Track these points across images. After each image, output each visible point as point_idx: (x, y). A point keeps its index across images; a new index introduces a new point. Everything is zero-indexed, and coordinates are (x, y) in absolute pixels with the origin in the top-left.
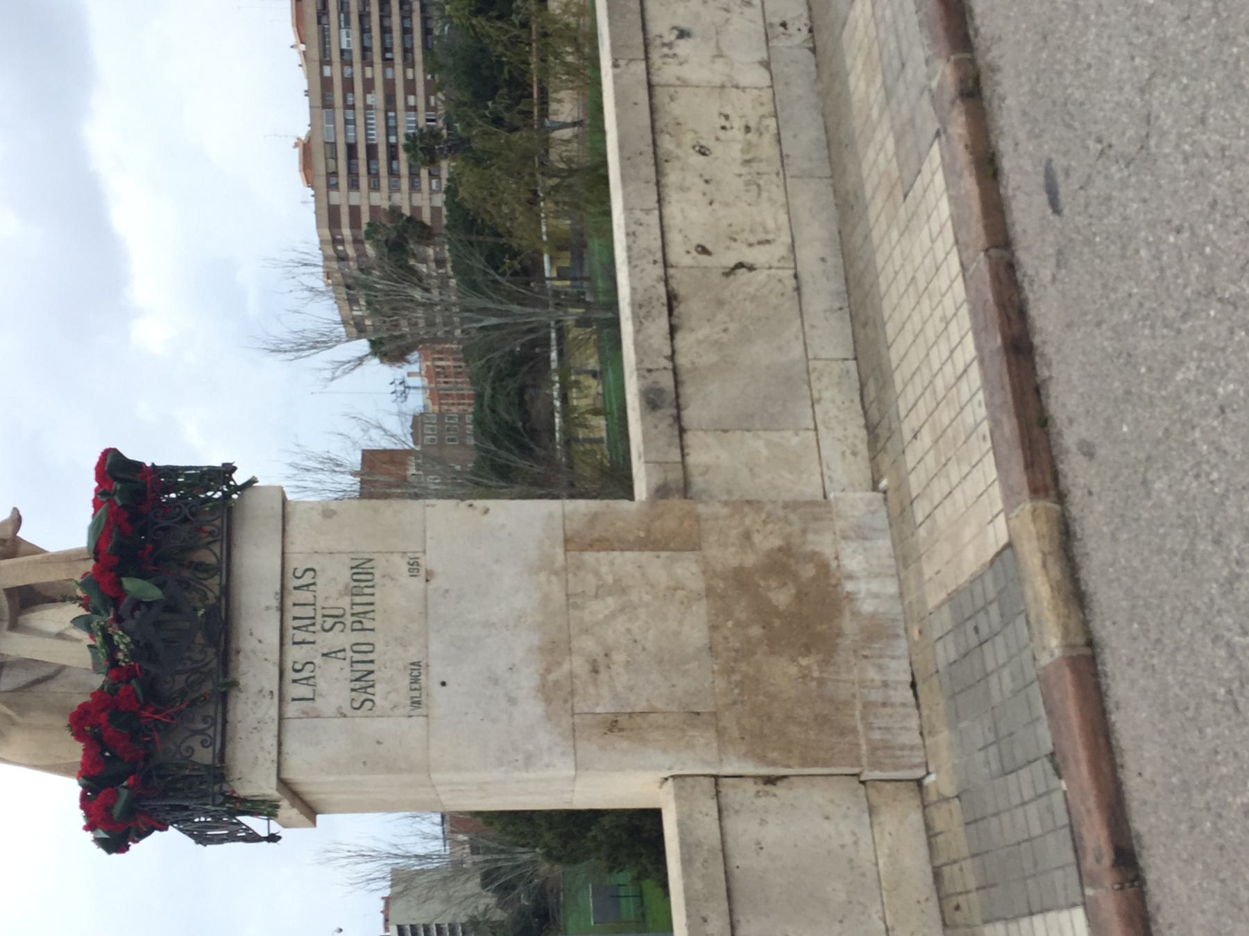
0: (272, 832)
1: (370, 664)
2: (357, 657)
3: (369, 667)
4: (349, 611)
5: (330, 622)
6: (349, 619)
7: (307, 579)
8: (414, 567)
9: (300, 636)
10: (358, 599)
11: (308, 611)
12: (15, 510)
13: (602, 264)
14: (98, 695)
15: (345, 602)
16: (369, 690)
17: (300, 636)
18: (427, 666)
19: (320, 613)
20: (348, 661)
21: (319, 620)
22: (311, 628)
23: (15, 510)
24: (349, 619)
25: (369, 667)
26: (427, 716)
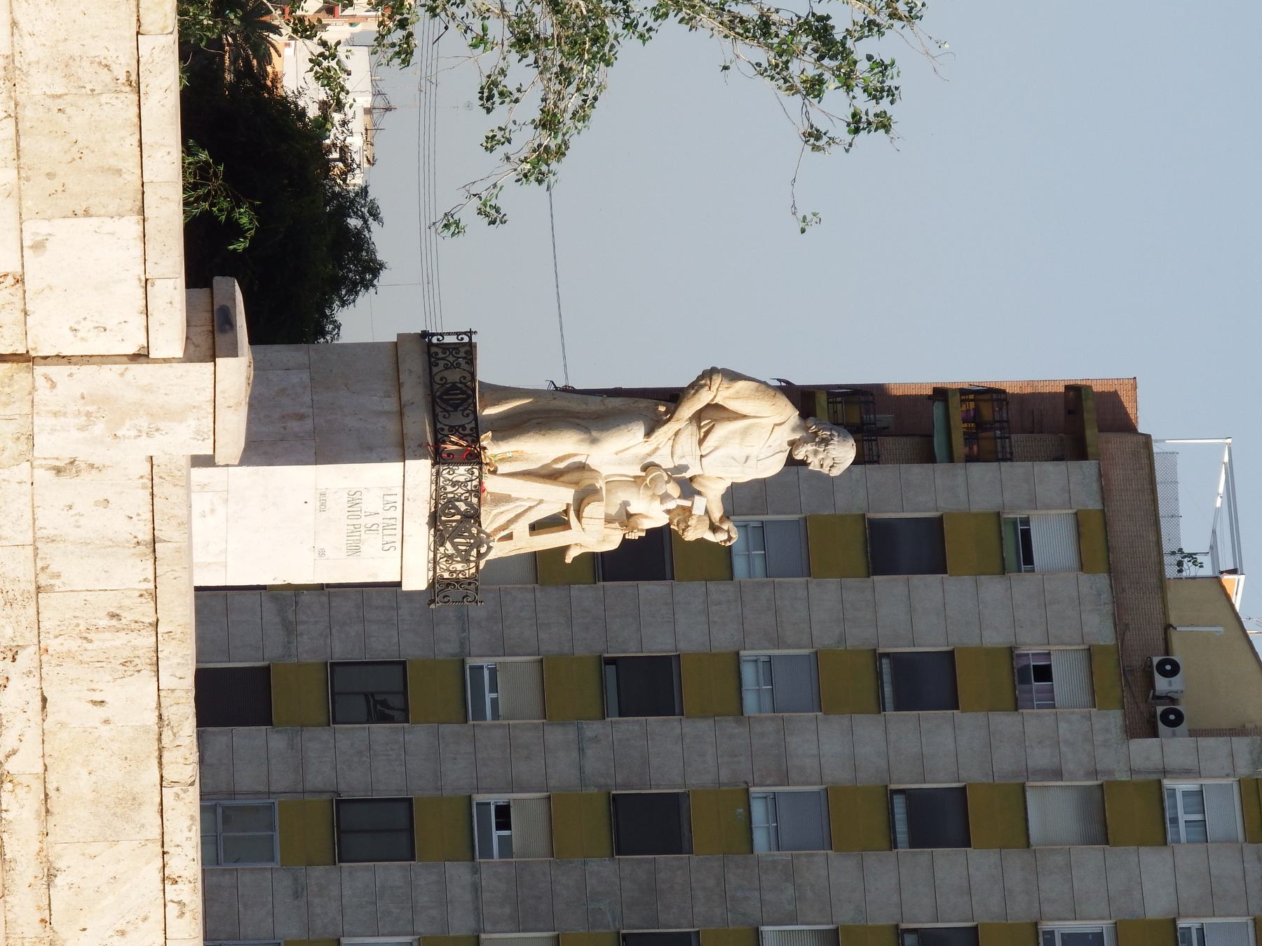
0: (209, 366)
1: (617, 449)
2: (359, 513)
3: (350, 509)
4: (362, 533)
5: (375, 527)
6: (363, 529)
7: (387, 547)
8: (322, 553)
9: (393, 521)
10: (358, 538)
11: (386, 532)
12: (489, 225)
13: (648, 434)
14: (565, 559)
15: (364, 536)
16: (350, 499)
17: (393, 521)
18: (315, 511)
19: (380, 531)
20: (363, 511)
21: (380, 528)
22: (384, 525)
23: (489, 225)
24: (363, 529)
25: (350, 509)
26: (316, 489)
